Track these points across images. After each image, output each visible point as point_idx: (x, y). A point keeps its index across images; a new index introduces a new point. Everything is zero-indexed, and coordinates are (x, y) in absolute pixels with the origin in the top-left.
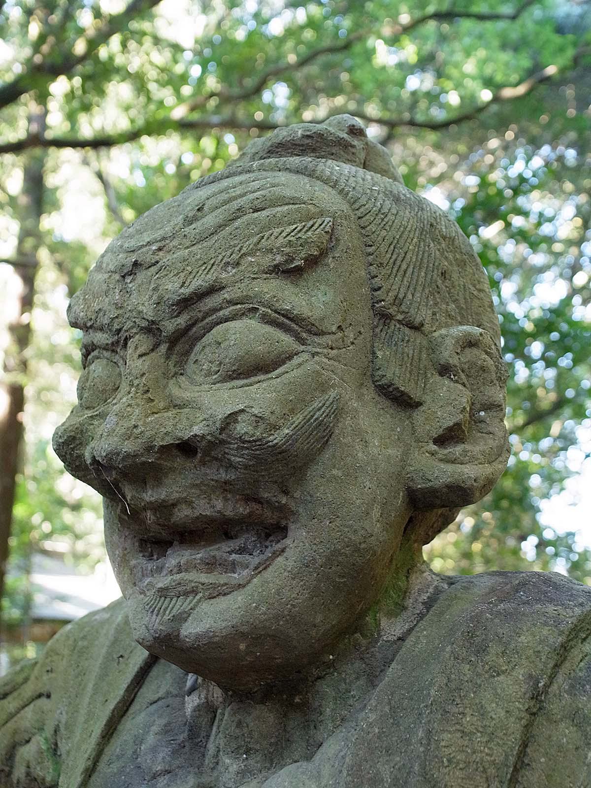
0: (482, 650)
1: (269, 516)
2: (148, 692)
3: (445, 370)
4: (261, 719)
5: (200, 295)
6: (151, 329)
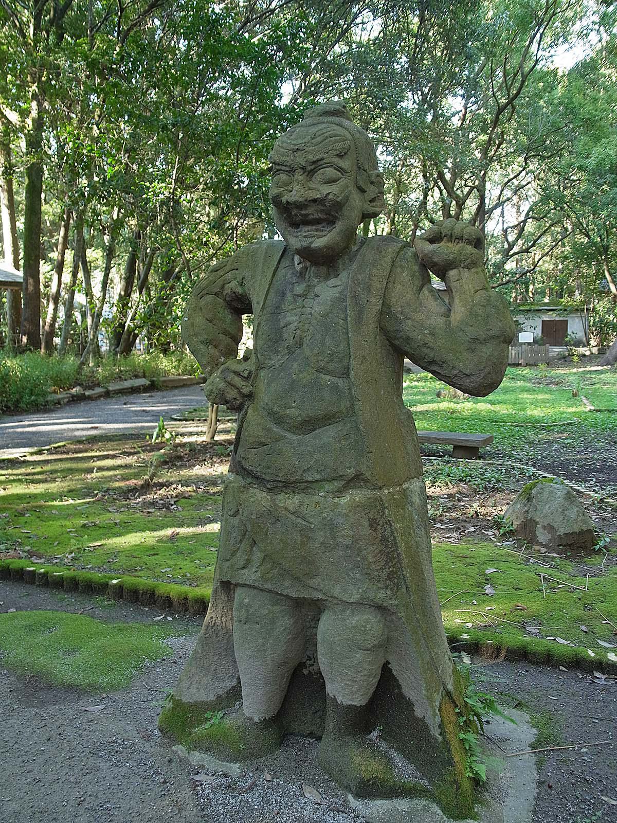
0: (381, 252)
1: (331, 219)
2: (282, 265)
3: (372, 183)
4: (323, 270)
5: (318, 161)
6: (303, 168)
